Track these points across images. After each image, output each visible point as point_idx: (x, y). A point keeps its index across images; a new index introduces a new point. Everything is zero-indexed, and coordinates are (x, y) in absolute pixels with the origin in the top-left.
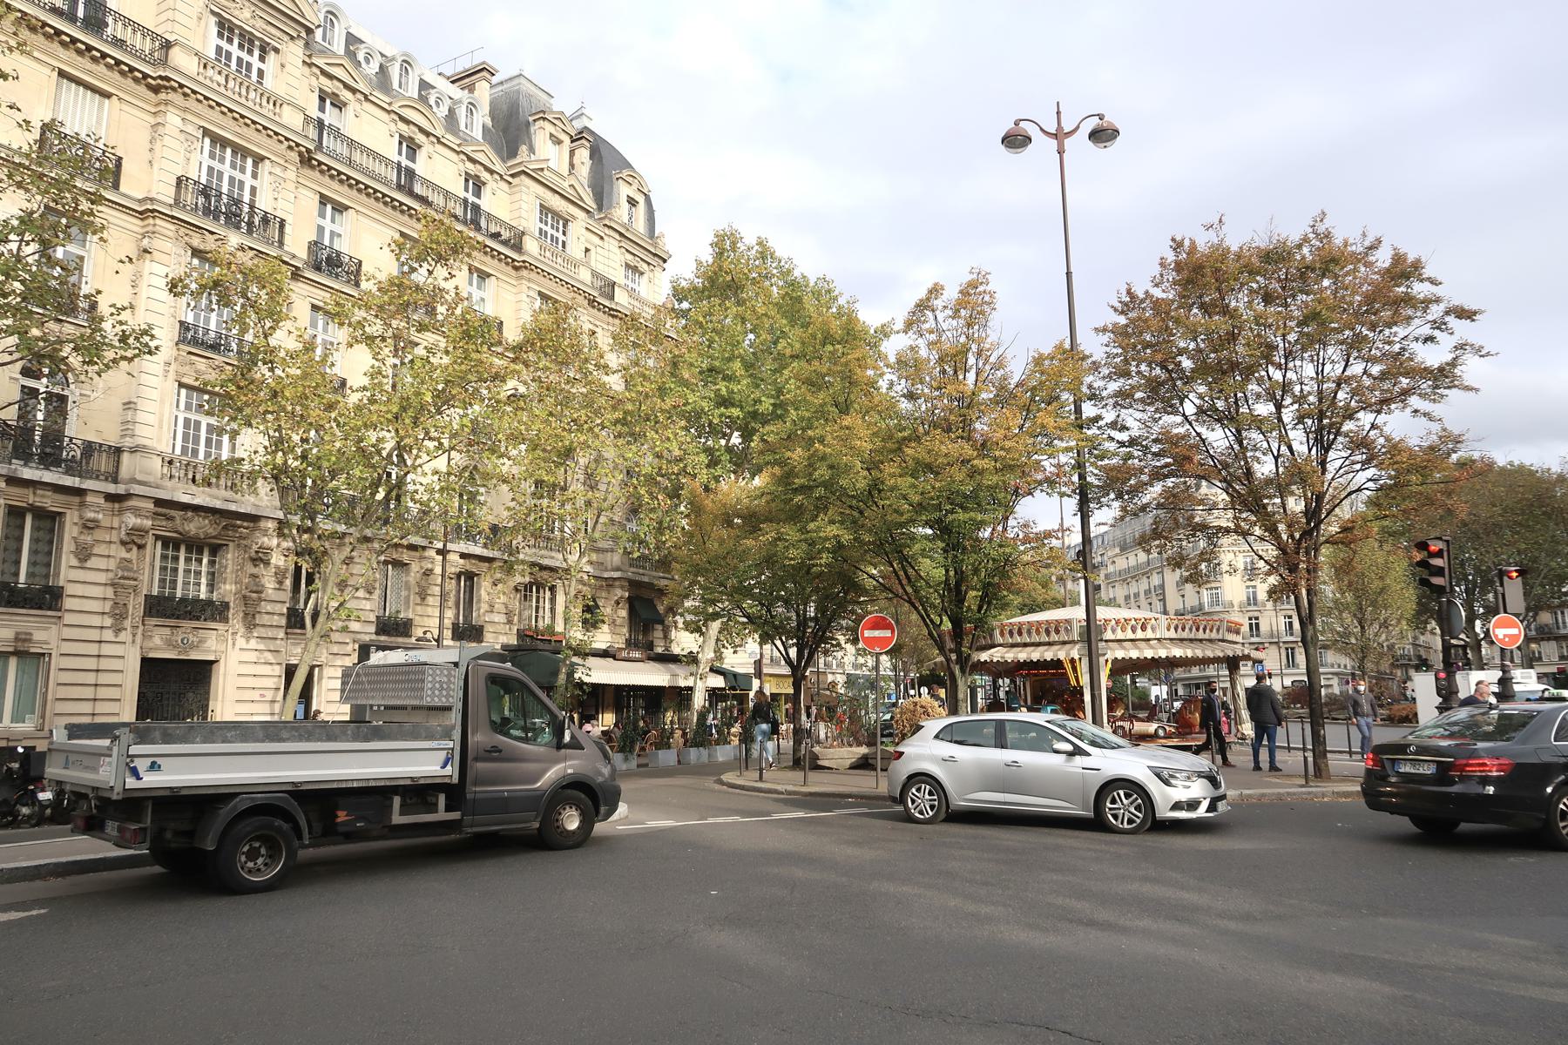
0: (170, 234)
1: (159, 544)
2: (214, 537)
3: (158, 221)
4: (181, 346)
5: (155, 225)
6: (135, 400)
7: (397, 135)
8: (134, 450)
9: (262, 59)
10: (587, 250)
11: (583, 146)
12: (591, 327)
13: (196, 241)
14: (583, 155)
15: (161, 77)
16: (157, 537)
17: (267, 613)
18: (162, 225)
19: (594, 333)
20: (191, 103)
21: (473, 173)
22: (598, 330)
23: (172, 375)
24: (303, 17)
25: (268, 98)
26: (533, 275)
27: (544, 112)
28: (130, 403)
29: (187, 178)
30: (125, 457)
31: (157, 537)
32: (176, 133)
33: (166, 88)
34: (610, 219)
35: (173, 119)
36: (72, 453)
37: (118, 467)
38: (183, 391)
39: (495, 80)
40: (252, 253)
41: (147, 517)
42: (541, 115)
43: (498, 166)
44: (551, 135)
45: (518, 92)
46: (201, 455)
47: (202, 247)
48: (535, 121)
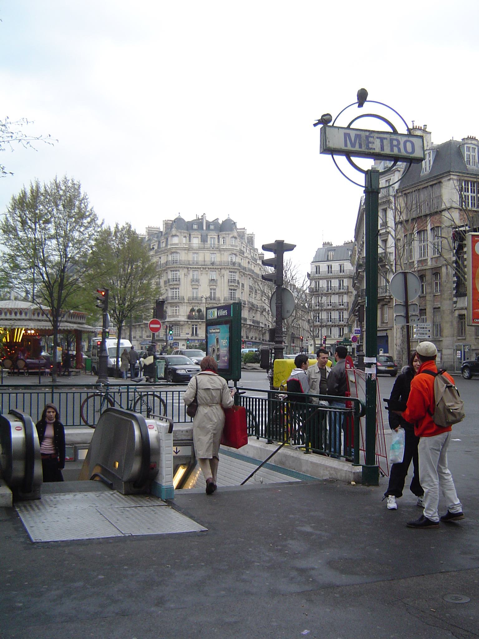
17: (219, 242)
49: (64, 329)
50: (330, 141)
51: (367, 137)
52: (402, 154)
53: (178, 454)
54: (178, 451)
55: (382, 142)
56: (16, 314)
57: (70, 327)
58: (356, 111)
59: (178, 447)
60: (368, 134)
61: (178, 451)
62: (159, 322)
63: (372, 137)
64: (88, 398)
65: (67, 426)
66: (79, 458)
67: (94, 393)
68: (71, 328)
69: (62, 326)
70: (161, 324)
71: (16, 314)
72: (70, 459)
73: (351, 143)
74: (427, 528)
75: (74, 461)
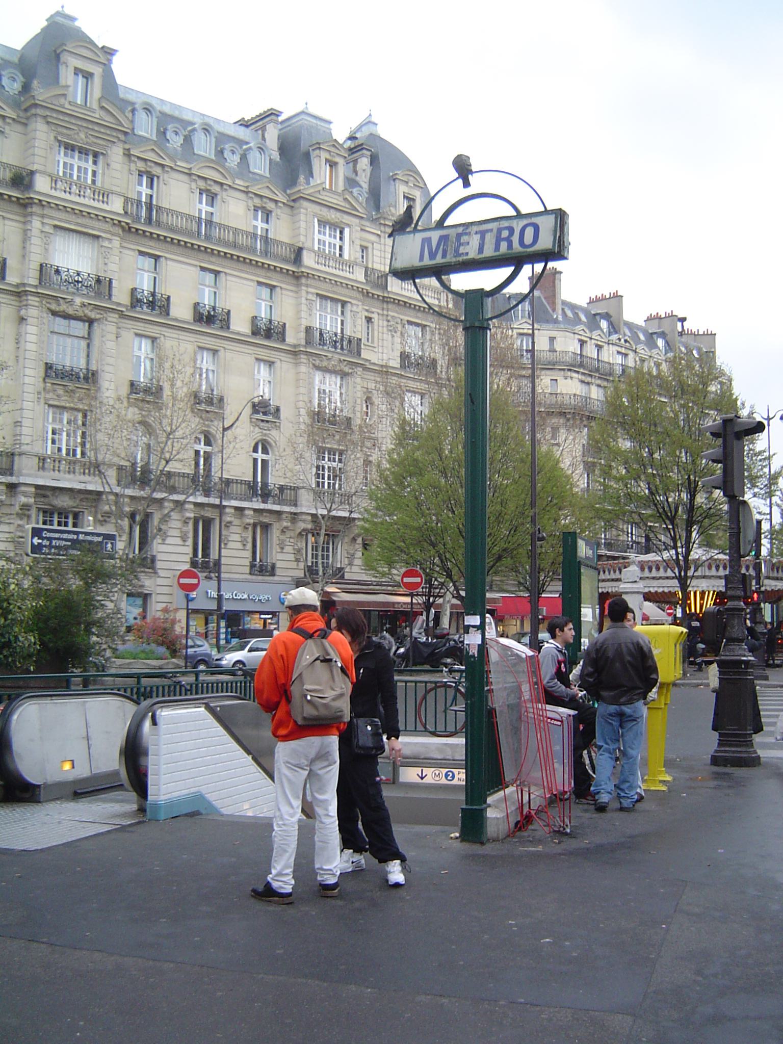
0: (37, 304)
1: (41, 515)
2: (74, 507)
3: (30, 297)
4: (47, 381)
5: (27, 300)
6: (20, 420)
7: (198, 190)
8: (20, 454)
9: (95, 163)
10: (364, 249)
11: (363, 155)
12: (366, 314)
13: (54, 307)
14: (364, 163)
15: (27, 198)
16: (39, 509)
18: (32, 300)
19: (371, 318)
20: (47, 211)
21: (259, 205)
22: (375, 316)
23: (42, 401)
24: (124, 127)
25: (99, 192)
26: (310, 282)
27: (319, 144)
28: (18, 422)
29: (46, 264)
30: (16, 458)
31: (39, 509)
32: (39, 234)
33: (31, 204)
34: (385, 219)
35: (36, 223)
36: (90, 283)
37: (13, 465)
38: (51, 410)
39: (280, 119)
40: (90, 307)
41: (31, 497)
42: (318, 146)
43: (281, 198)
44: (327, 160)
45: (301, 126)
46: (75, 178)
47: (57, 309)
48: (313, 150)
49: (670, 592)
50: (398, 258)
51: (459, 236)
52: (517, 251)
53: (424, 781)
54: (424, 775)
55: (483, 239)
56: (650, 569)
57: (770, 586)
58: (458, 191)
59: (424, 769)
60: (460, 230)
61: (424, 775)
62: (197, 575)
63: (466, 234)
64: (427, 692)
65: (406, 730)
66: (401, 780)
67: (436, 683)
68: (773, 588)
69: (693, 587)
70: (201, 578)
71: (650, 569)
72: (387, 780)
73: (429, 253)
74: (270, 901)
75: (394, 783)
